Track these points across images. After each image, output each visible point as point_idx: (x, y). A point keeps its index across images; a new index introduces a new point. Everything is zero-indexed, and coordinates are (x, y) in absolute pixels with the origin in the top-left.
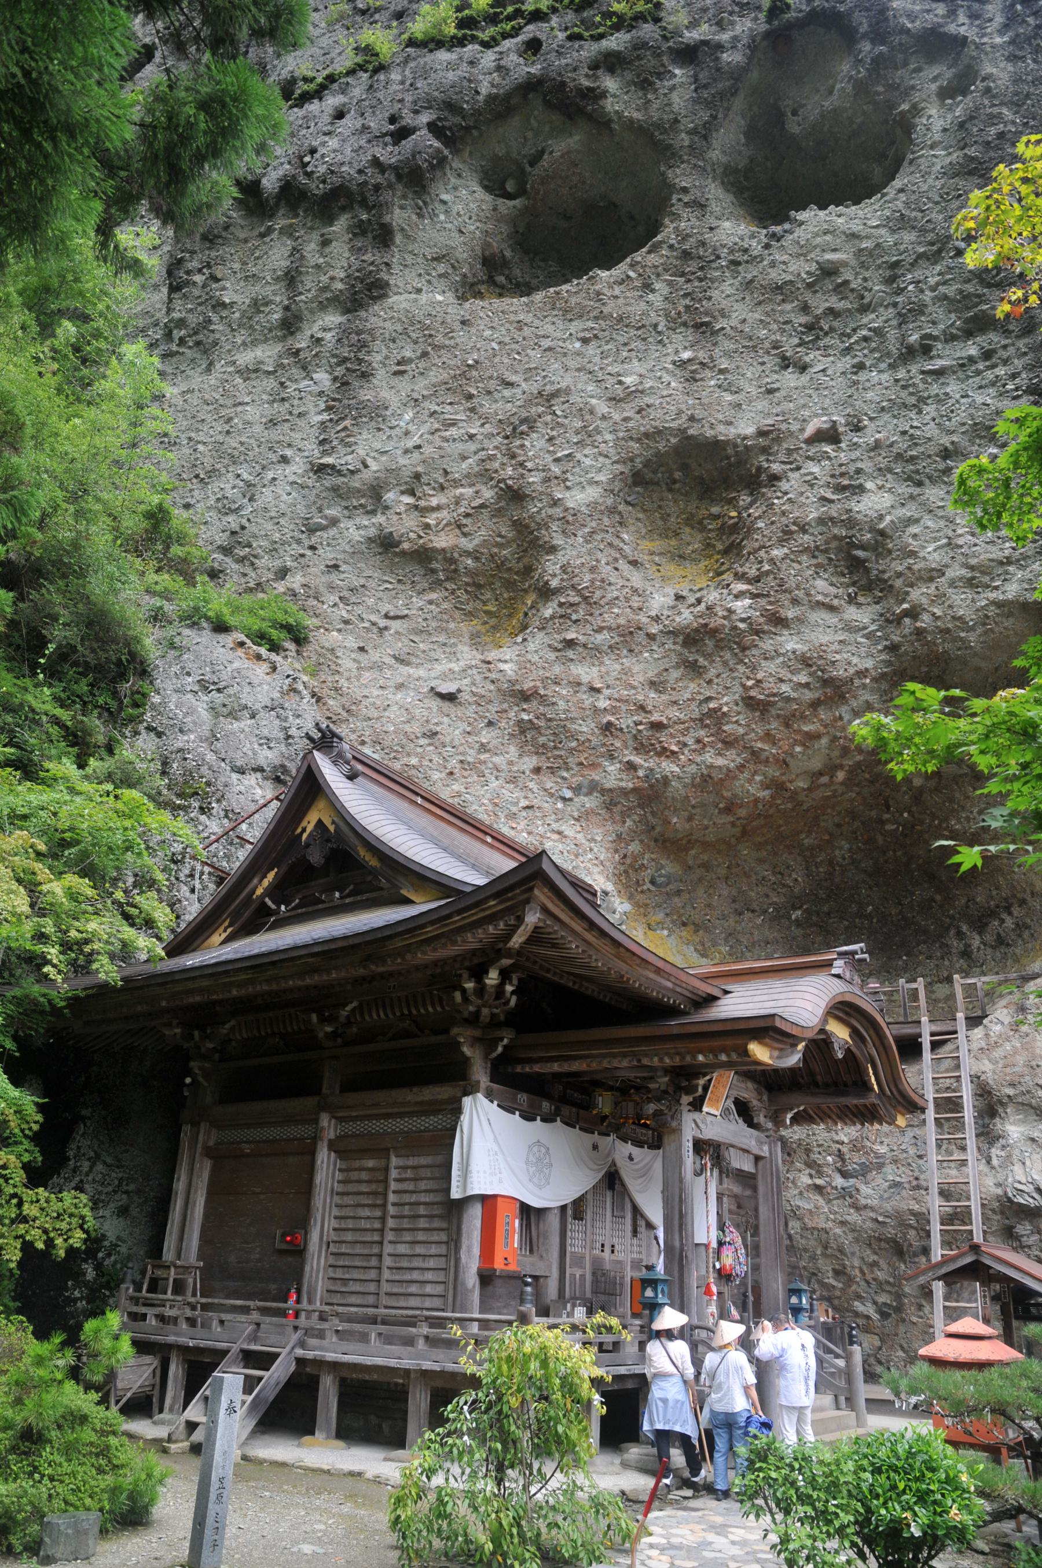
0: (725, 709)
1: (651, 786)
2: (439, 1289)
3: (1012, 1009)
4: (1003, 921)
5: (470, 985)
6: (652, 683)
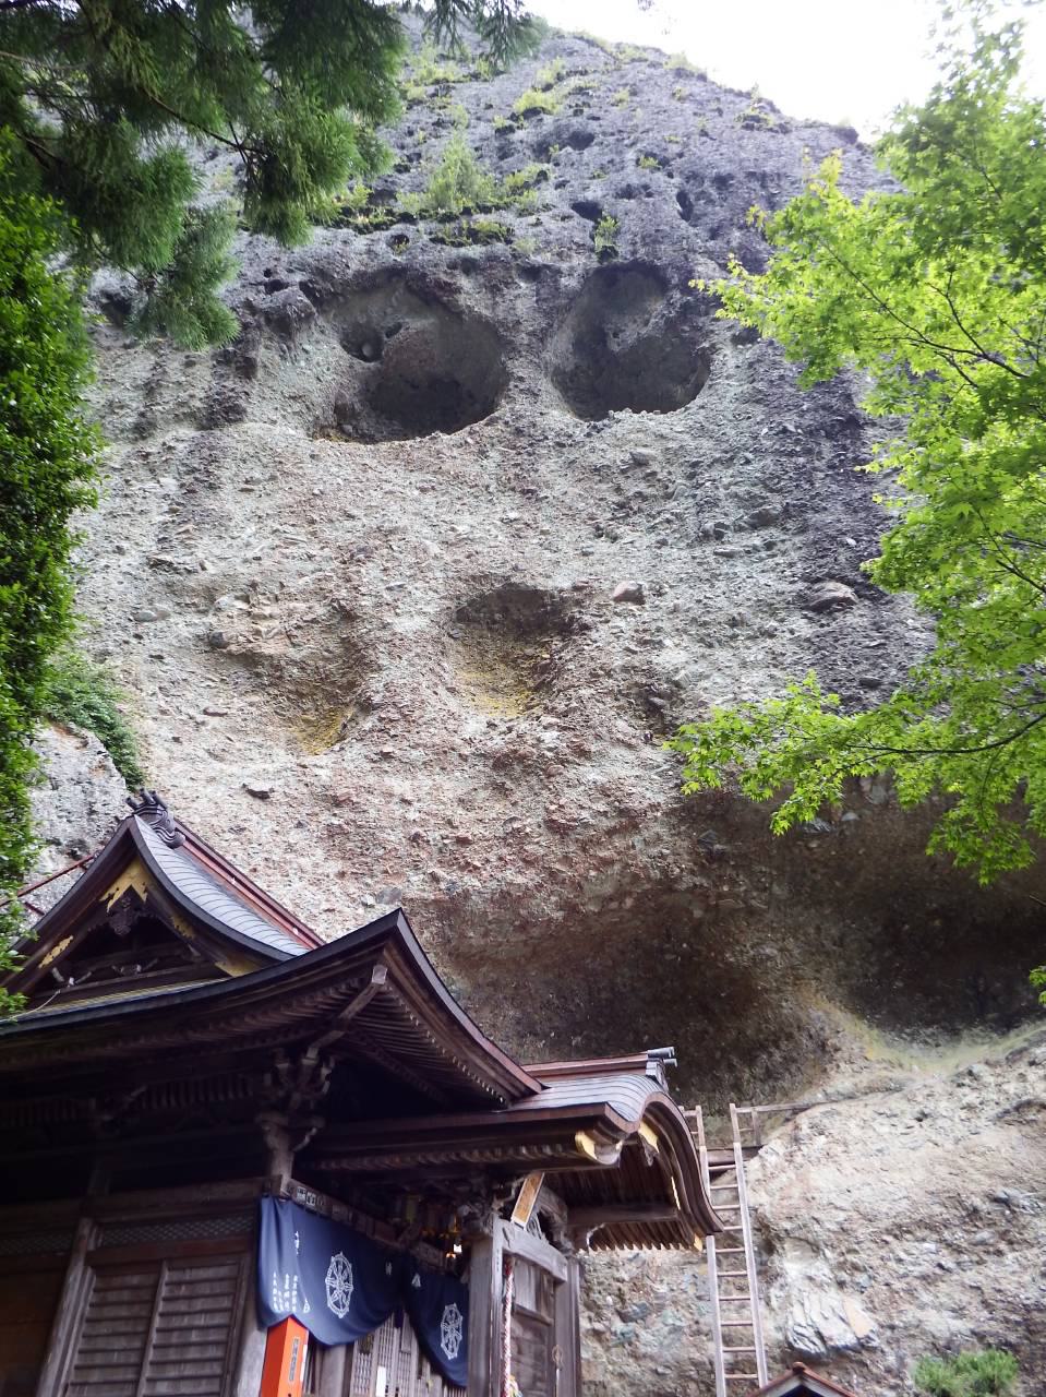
0: (528, 830)
1: (452, 899)
4: (771, 1055)
5: (283, 1066)
6: (461, 801)
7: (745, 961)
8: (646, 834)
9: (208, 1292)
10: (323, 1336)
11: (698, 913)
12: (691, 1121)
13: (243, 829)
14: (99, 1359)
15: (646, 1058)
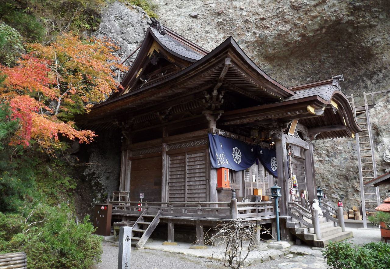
0: (285, 11)
1: (261, 39)
2: (204, 195)
3: (384, 102)
4: (378, 75)
5: (207, 96)
6: (260, 5)
7: (369, 45)
8: (329, 4)
9: (198, 160)
10: (234, 168)
11: (350, 30)
12: (350, 99)
13: (191, 29)
14: (175, 177)
15: (332, 79)
